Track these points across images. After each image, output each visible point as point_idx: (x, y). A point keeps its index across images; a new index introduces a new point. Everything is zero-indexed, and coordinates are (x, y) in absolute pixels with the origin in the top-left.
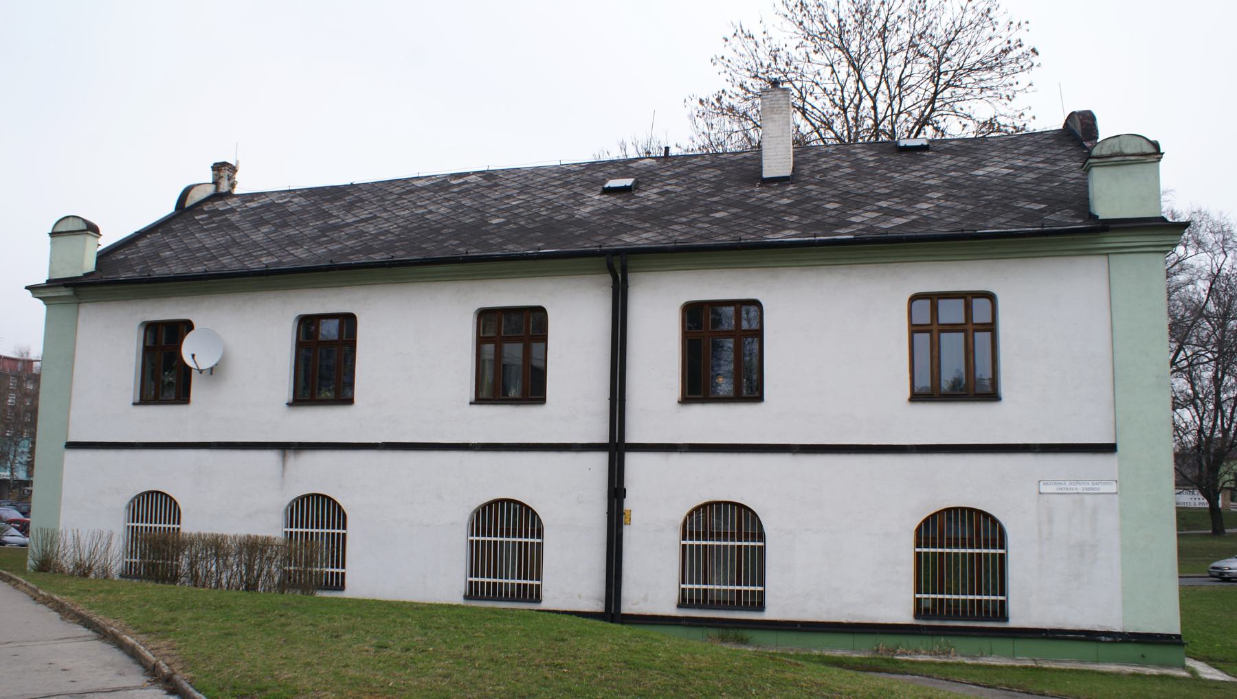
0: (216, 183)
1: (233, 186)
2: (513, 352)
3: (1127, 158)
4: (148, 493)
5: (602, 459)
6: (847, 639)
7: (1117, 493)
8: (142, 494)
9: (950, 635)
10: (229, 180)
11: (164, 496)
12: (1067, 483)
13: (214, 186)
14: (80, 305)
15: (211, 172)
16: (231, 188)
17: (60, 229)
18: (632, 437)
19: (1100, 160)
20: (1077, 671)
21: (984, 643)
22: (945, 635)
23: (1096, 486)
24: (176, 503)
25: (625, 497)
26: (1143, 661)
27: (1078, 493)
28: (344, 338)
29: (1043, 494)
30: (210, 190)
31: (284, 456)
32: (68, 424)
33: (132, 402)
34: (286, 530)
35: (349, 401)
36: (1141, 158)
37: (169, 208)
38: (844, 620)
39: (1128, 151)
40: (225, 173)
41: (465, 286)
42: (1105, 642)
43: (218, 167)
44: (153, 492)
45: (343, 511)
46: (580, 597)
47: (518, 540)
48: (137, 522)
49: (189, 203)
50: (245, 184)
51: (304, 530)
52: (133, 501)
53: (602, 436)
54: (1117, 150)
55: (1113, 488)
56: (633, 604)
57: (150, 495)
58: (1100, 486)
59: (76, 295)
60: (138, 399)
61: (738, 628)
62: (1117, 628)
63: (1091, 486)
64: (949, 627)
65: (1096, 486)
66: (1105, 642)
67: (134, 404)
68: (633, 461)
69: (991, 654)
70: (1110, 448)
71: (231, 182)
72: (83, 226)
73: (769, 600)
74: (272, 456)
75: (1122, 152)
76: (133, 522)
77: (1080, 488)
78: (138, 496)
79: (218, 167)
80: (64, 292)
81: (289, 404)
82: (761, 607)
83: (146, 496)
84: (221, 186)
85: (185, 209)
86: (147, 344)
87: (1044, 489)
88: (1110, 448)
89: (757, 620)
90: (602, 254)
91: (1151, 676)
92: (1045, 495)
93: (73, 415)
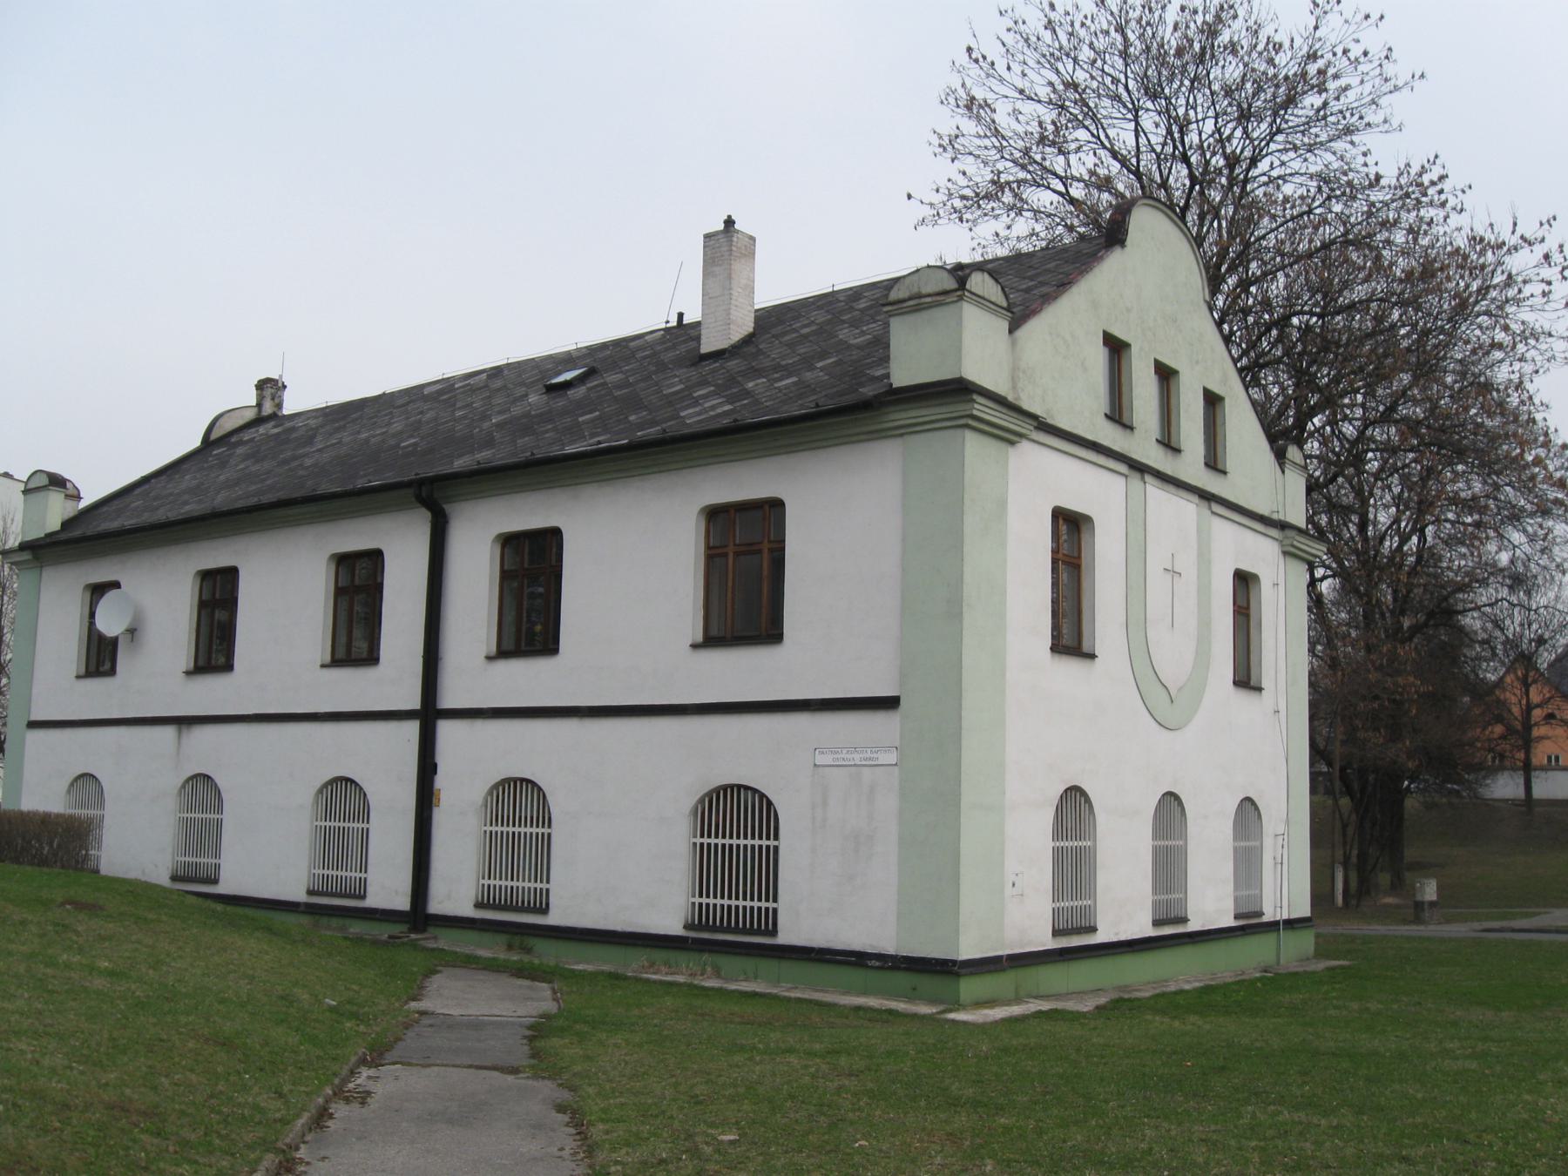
0: (259, 405)
1: (280, 406)
2: (220, 615)
3: (923, 300)
4: (725, 788)
5: (412, 729)
6: (472, 935)
7: (896, 764)
8: (717, 790)
9: (717, 952)
10: (273, 399)
11: (529, 785)
12: (845, 751)
13: (256, 409)
14: (44, 569)
15: (255, 392)
16: (275, 409)
17: (31, 485)
18: (448, 700)
19: (895, 307)
20: (810, 1001)
21: (749, 963)
22: (711, 951)
23: (875, 755)
24: (770, 803)
25: (436, 773)
26: (912, 995)
27: (855, 765)
28: (217, 596)
29: (819, 766)
30: (250, 415)
31: (180, 732)
32: (30, 700)
33: (75, 674)
34: (695, 840)
35: (228, 667)
36: (938, 298)
37: (195, 442)
38: (619, 928)
39: (925, 291)
40: (268, 392)
41: (322, 529)
42: (872, 967)
43: (262, 385)
44: (732, 787)
45: (775, 811)
46: (397, 892)
47: (757, 842)
48: (738, 837)
49: (214, 435)
50: (293, 404)
51: (720, 841)
52: (701, 801)
53: (414, 703)
54: (915, 290)
55: (892, 758)
56: (440, 903)
57: (722, 792)
58: (879, 755)
59: (36, 558)
60: (83, 671)
61: (522, 934)
62: (890, 949)
63: (869, 755)
64: (764, 944)
65: (875, 755)
66: (872, 967)
67: (78, 677)
68: (445, 729)
69: (756, 978)
70: (890, 703)
71: (277, 401)
72: (44, 481)
73: (371, 890)
74: (169, 732)
75: (920, 292)
76: (702, 836)
77: (857, 758)
78: (709, 794)
79: (262, 385)
80: (26, 556)
81: (188, 673)
82: (544, 910)
83: (722, 792)
84: (264, 409)
85: (214, 443)
86: (204, 598)
87: (820, 760)
88: (890, 703)
89: (541, 926)
90: (408, 484)
91: (712, 989)
92: (821, 769)
93: (35, 691)
